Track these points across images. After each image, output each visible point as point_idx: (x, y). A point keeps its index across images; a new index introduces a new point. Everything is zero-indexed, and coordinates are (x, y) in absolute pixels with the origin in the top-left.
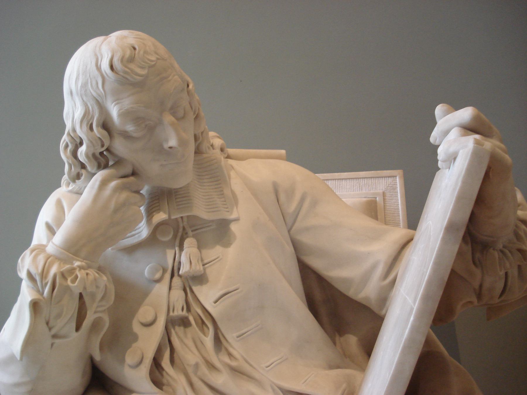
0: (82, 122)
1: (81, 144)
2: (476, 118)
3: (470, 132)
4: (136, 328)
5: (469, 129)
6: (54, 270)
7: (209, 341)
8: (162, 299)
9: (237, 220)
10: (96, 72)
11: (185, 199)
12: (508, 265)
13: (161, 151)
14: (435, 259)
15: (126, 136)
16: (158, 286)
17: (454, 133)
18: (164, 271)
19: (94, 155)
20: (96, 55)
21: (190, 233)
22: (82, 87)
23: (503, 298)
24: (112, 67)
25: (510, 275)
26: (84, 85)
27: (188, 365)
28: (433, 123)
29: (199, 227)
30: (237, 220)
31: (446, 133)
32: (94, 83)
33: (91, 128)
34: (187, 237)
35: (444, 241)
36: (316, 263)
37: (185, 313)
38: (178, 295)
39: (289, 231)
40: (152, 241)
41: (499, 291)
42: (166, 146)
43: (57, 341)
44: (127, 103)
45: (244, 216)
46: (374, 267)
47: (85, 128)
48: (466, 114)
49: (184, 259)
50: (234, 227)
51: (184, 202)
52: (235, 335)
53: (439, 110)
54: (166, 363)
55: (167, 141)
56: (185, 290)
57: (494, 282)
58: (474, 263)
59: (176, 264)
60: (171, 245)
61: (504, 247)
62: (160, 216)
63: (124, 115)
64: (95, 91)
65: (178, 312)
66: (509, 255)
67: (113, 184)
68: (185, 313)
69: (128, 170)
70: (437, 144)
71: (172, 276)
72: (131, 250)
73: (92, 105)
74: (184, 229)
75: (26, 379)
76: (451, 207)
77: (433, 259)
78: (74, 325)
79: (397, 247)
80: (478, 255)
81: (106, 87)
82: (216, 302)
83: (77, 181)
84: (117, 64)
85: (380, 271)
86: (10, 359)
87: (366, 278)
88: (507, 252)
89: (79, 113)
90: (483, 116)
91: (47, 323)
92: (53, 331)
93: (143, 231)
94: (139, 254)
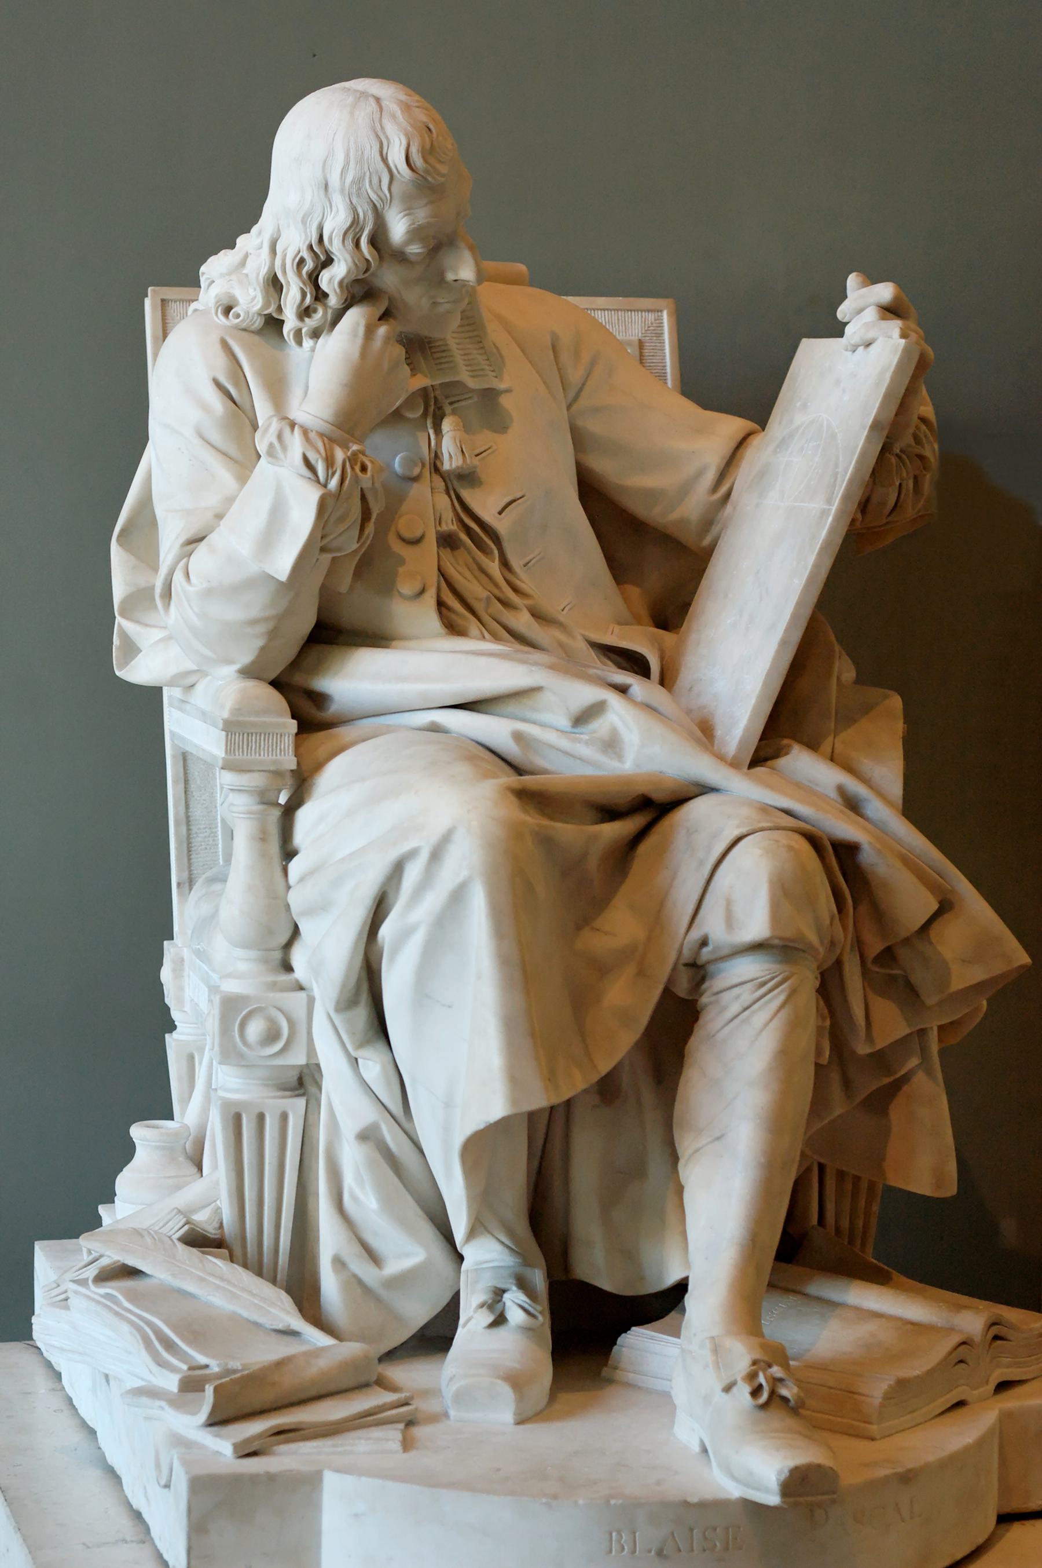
1: (329, 261)
2: (896, 299)
3: (892, 316)
4: (397, 547)
5: (890, 310)
6: (340, 455)
8: (428, 508)
9: (508, 391)
10: (381, 165)
11: (444, 354)
12: (905, 474)
14: (857, 462)
15: (400, 257)
16: (415, 485)
17: (870, 314)
21: (448, 409)
22: (353, 182)
23: (890, 519)
25: (904, 485)
26: (358, 181)
27: (476, 599)
29: (456, 399)
30: (508, 391)
31: (860, 311)
32: (375, 180)
33: (357, 244)
35: (868, 439)
42: (450, 276)
44: (422, 215)
45: (520, 386)
46: (701, 473)
48: (885, 291)
49: (448, 446)
50: (505, 401)
51: (443, 360)
52: (522, 563)
53: (852, 281)
61: (901, 451)
63: (415, 234)
64: (376, 193)
66: (907, 461)
70: (845, 321)
73: (364, 211)
75: (272, 612)
76: (877, 405)
77: (854, 462)
79: (733, 445)
82: (500, 513)
83: (307, 320)
84: (418, 161)
85: (711, 476)
87: (686, 489)
88: (904, 457)
90: (903, 295)
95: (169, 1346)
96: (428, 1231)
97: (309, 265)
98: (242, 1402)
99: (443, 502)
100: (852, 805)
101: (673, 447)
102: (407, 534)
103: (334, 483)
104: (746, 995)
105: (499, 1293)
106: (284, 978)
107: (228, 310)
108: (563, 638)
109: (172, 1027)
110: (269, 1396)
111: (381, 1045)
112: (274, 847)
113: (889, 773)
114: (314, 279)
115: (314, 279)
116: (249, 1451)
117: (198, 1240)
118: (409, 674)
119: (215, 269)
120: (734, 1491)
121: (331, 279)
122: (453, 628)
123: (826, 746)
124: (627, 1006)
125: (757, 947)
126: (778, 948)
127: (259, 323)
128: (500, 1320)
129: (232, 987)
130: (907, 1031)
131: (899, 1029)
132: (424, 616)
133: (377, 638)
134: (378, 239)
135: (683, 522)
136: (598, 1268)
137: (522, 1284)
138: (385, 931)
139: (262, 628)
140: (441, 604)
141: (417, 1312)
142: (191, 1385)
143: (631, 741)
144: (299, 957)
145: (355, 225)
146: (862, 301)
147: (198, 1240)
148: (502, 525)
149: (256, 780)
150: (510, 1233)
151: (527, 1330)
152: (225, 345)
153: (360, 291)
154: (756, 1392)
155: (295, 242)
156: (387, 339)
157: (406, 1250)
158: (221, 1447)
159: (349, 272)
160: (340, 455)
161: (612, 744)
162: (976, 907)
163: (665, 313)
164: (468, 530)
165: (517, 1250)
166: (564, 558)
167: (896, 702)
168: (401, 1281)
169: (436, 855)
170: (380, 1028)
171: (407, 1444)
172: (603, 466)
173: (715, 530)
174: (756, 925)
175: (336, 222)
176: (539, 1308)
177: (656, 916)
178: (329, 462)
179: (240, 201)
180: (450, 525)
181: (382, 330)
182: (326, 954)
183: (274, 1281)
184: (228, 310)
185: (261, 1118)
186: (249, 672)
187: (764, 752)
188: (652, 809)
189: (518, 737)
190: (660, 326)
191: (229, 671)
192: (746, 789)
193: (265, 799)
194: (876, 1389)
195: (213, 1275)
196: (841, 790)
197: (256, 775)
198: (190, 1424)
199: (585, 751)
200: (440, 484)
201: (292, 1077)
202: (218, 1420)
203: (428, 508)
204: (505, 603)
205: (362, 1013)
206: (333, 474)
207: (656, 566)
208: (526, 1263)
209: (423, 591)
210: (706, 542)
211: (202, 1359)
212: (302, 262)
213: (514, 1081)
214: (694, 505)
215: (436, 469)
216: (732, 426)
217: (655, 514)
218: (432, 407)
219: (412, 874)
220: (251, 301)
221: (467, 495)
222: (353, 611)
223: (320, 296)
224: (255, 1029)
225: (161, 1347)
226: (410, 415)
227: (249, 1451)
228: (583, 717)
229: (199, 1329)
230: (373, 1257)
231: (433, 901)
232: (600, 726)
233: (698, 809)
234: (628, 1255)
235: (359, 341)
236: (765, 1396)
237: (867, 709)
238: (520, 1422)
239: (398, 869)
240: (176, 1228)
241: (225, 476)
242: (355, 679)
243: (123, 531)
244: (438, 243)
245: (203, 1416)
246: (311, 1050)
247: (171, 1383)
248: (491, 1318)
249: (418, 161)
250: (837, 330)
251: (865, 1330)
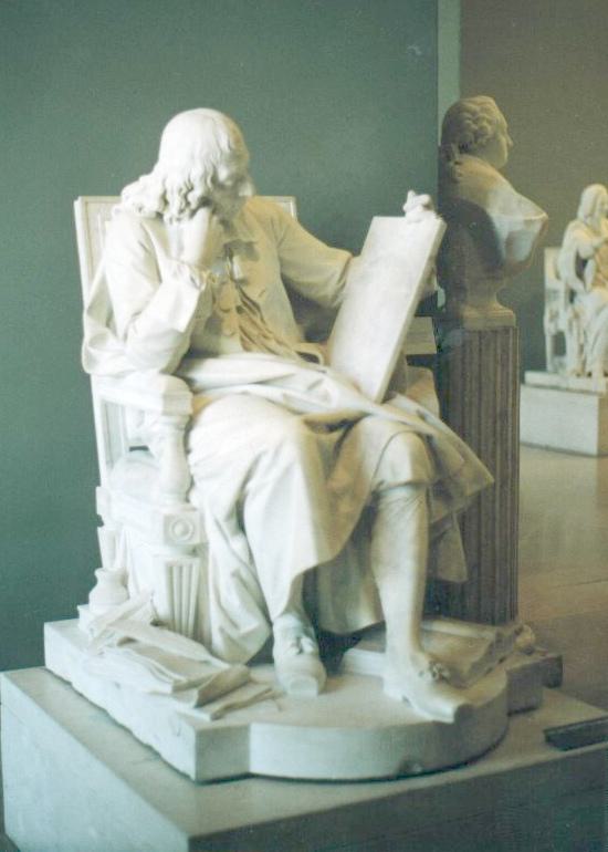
4: (221, 314)
6: (205, 275)
8: (231, 297)
17: (419, 209)
21: (235, 252)
24: (229, 147)
31: (413, 207)
33: (206, 181)
35: (428, 264)
42: (241, 194)
44: (234, 169)
50: (256, 247)
63: (230, 177)
85: (337, 276)
87: (326, 284)
95: (162, 673)
96: (258, 613)
97: (184, 191)
98: (209, 695)
99: (236, 293)
100: (423, 417)
101: (321, 262)
102: (225, 308)
104: (402, 504)
105: (298, 639)
106: (188, 506)
107: (140, 209)
109: (101, 524)
111: (241, 534)
112: (182, 449)
113: (433, 402)
114: (185, 197)
115: (185, 197)
116: (216, 717)
117: (157, 623)
118: (228, 369)
119: (130, 191)
120: (429, 717)
121: (194, 197)
122: (246, 349)
123: (407, 392)
124: (350, 510)
125: (408, 484)
126: (414, 484)
127: (154, 215)
128: (301, 651)
129: (166, 511)
131: (444, 513)
132: (235, 344)
134: (214, 180)
135: (326, 297)
136: (331, 625)
137: (307, 634)
138: (251, 486)
139: (171, 353)
140: (242, 340)
141: (253, 648)
142: (179, 689)
143: (333, 398)
144: (195, 497)
146: (415, 203)
147: (157, 623)
148: (260, 302)
149: (175, 419)
150: (298, 611)
151: (312, 654)
152: (142, 227)
153: (205, 202)
154: (434, 675)
155: (175, 182)
157: (250, 623)
158: (204, 717)
161: (326, 397)
164: (245, 304)
165: (301, 619)
166: (279, 314)
167: (429, 373)
168: (246, 637)
169: (277, 453)
170: (241, 527)
171: (280, 708)
172: (292, 274)
173: (339, 300)
174: (406, 474)
175: (196, 172)
177: (358, 472)
178: (201, 277)
179: (146, 160)
180: (240, 303)
181: (215, 218)
182: (214, 498)
183: (187, 636)
184: (140, 209)
185: (181, 568)
186: (164, 372)
187: (387, 398)
188: (346, 426)
189: (285, 396)
191: (155, 371)
192: (383, 412)
193: (177, 427)
194: (466, 668)
196: (418, 412)
198: (186, 707)
199: (315, 401)
200: (234, 284)
201: (191, 549)
202: (201, 704)
203: (231, 297)
204: (265, 337)
205: (234, 521)
207: (316, 320)
208: (307, 626)
209: (233, 334)
210: (336, 304)
211: (177, 677)
212: (181, 190)
213: (319, 550)
214: (330, 290)
215: (232, 278)
216: (345, 254)
217: (313, 294)
218: (229, 252)
219: (265, 461)
220: (153, 205)
221: (244, 289)
222: (206, 341)
223: (188, 204)
224: (179, 529)
225: (157, 673)
229: (171, 663)
230: (235, 625)
231: (276, 472)
233: (366, 424)
234: (342, 617)
235: (206, 225)
236: (437, 677)
237: (420, 376)
239: (256, 462)
240: (148, 619)
241: (146, 285)
242: (206, 372)
243: (90, 308)
244: (238, 180)
245: (193, 703)
246: (203, 535)
247: (168, 689)
248: (298, 650)
249: (233, 146)
250: (402, 213)
251: (450, 641)
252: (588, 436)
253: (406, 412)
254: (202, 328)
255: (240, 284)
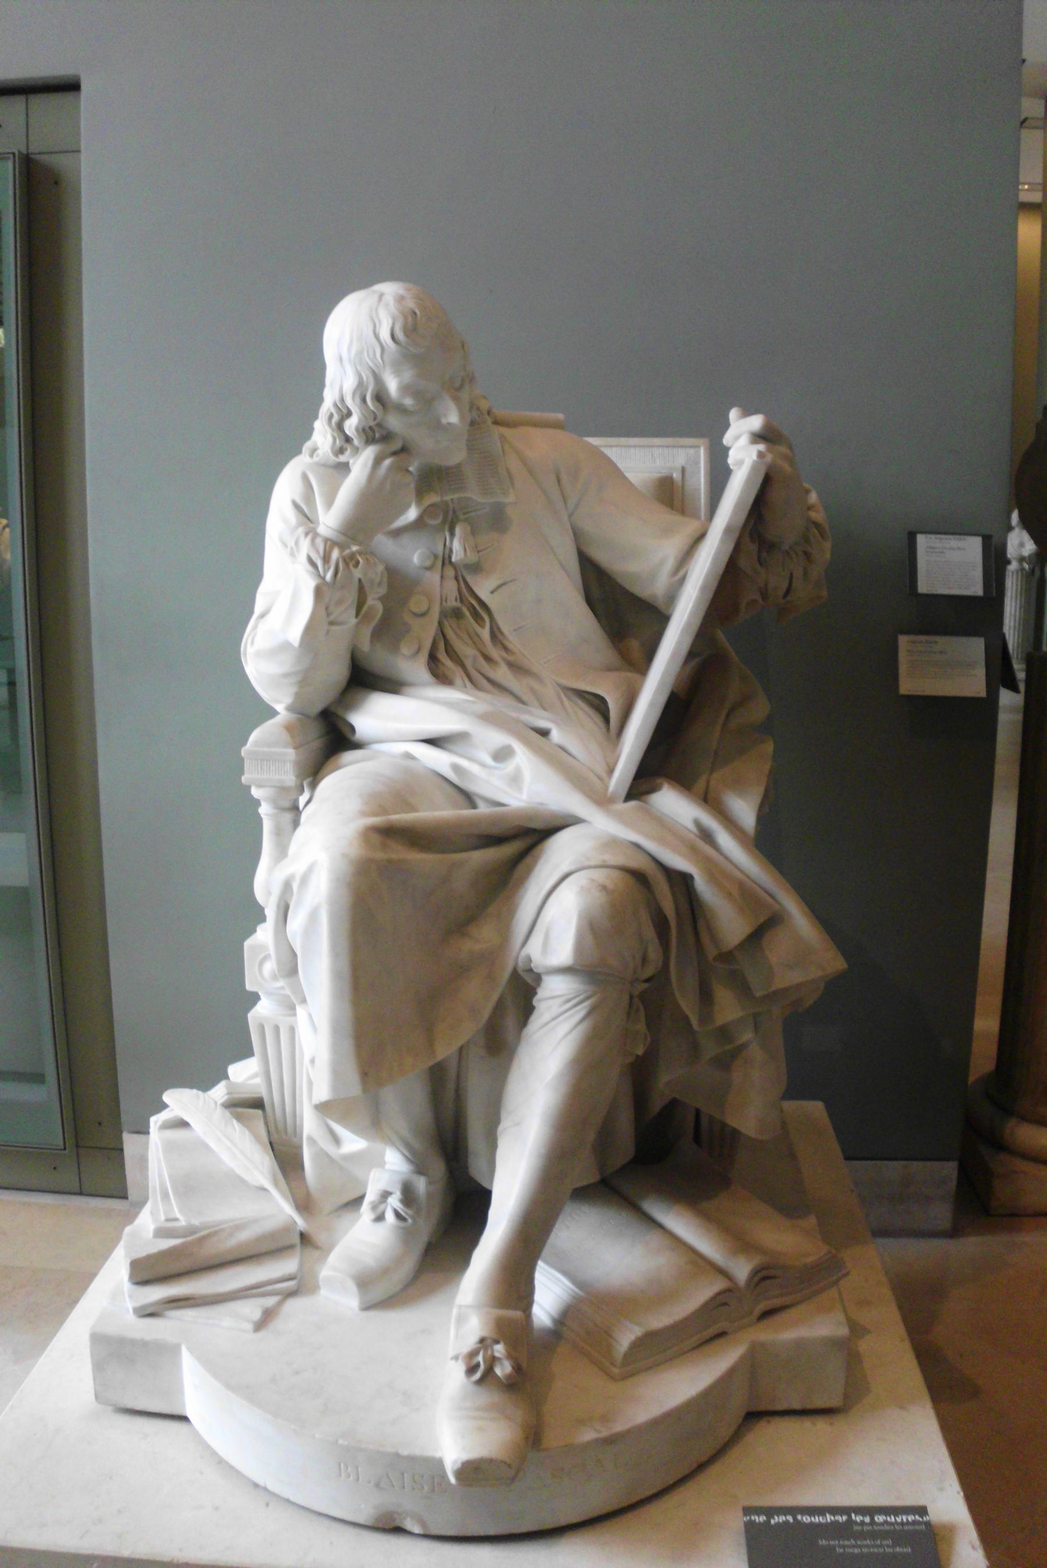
0: (354, 394)
1: (349, 414)
4: (407, 618)
5: (758, 437)
6: (335, 554)
7: (485, 633)
8: (440, 589)
13: (437, 426)
15: (401, 409)
17: (744, 440)
18: (436, 557)
19: (364, 430)
20: (373, 320)
23: (789, 598)
24: (393, 337)
26: (360, 353)
28: (726, 425)
31: (737, 438)
32: (371, 353)
33: (364, 400)
34: (458, 521)
36: (601, 556)
37: (459, 604)
38: (451, 586)
39: (570, 516)
40: (419, 524)
41: (781, 592)
42: (444, 421)
43: (335, 628)
47: (358, 400)
48: (756, 422)
49: (457, 545)
53: (733, 414)
54: (442, 656)
55: (446, 415)
56: (456, 578)
57: (777, 582)
58: (761, 564)
59: (447, 551)
60: (439, 529)
61: (790, 548)
62: (433, 498)
63: (405, 389)
65: (452, 603)
67: (387, 462)
68: (459, 604)
69: (397, 446)
71: (443, 564)
72: (397, 533)
73: (366, 376)
74: (454, 512)
78: (354, 612)
80: (764, 554)
81: (386, 358)
82: (492, 592)
86: (286, 646)
89: (349, 383)
91: (327, 608)
92: (332, 618)
93: (412, 514)
94: (406, 539)
103: (329, 576)
108: (535, 685)
110: (185, 1264)
115: (340, 427)
121: (351, 425)
122: (441, 678)
123: (700, 785)
124: (479, 997)
128: (380, 1218)
130: (741, 1014)
132: (415, 669)
133: (392, 686)
134: (381, 398)
145: (361, 385)
150: (408, 1145)
156: (390, 468)
159: (360, 420)
160: (335, 554)
161: (515, 780)
162: (800, 921)
163: (702, 451)
176: (410, 1212)
178: (326, 559)
185: (277, 1029)
189: (456, 768)
190: (699, 456)
195: (228, 1138)
196: (697, 823)
197: (267, 789)
204: (488, 659)
206: (329, 568)
212: (331, 416)
222: (380, 659)
226: (432, 522)
227: (150, 1313)
228: (502, 755)
232: (510, 767)
238: (368, 1307)
252: (1038, 241)
253: (664, 825)
254: (367, 632)
255: (463, 575)
